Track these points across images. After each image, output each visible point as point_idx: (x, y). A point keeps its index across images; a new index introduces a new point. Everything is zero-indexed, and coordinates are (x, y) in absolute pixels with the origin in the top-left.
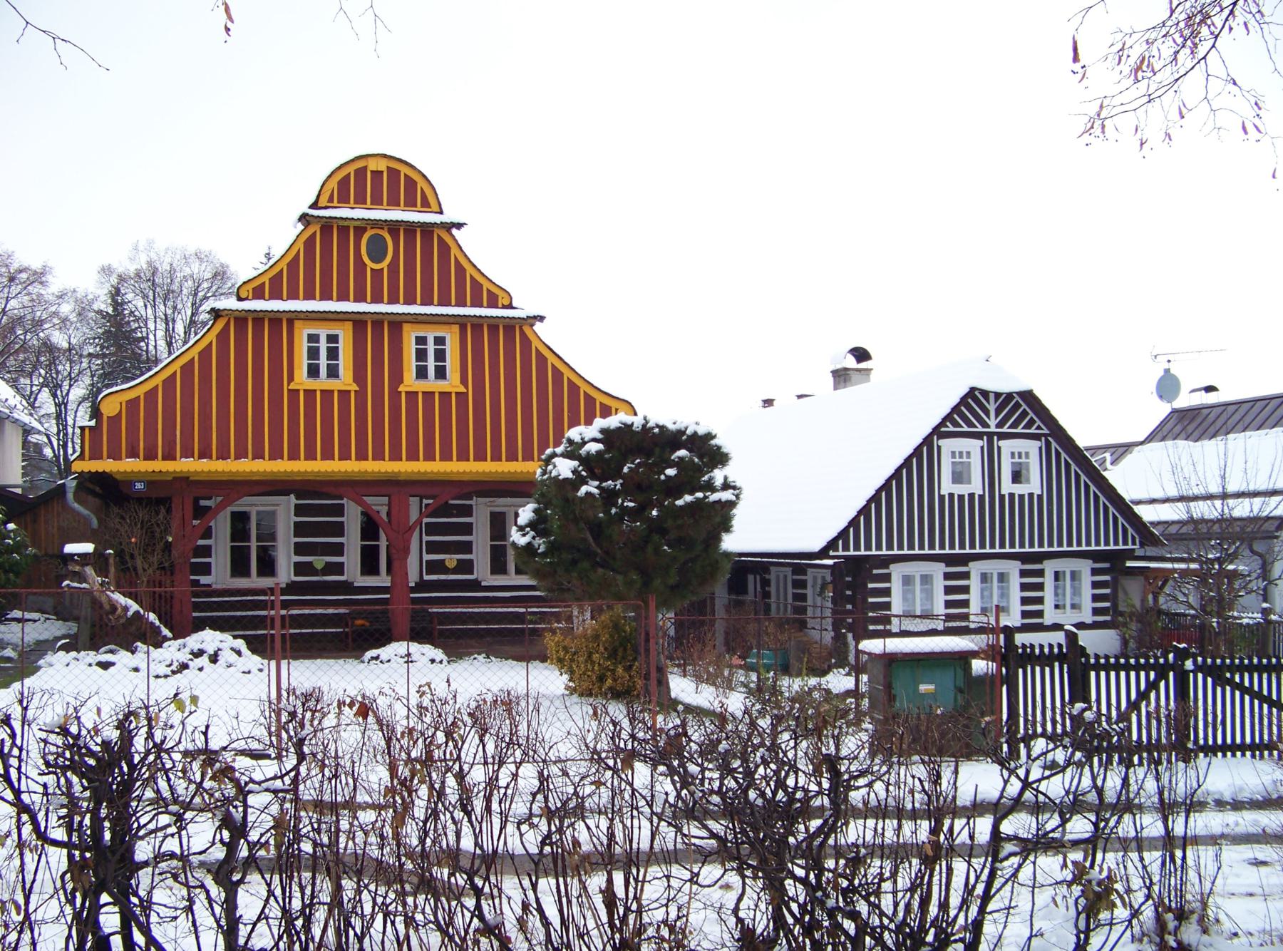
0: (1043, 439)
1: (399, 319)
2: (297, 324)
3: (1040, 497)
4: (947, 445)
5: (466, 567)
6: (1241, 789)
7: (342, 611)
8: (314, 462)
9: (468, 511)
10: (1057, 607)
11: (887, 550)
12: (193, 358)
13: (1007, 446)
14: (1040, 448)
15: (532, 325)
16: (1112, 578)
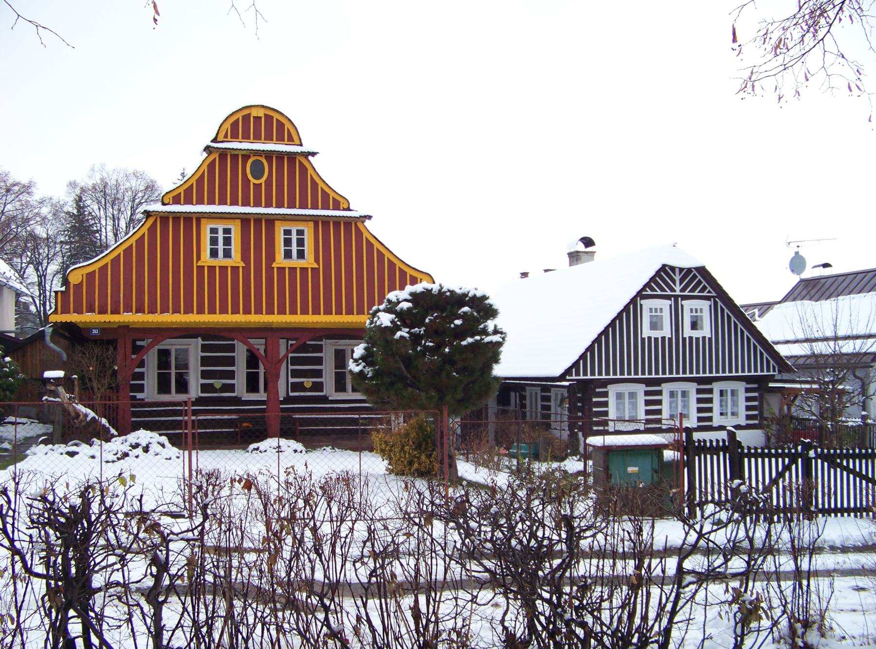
0: (712, 299)
1: (272, 217)
2: (203, 221)
3: (710, 339)
4: (647, 304)
5: (318, 387)
6: (847, 539)
7: (233, 417)
8: (214, 315)
9: (319, 349)
10: (722, 414)
11: (606, 375)
12: (132, 244)
13: (687, 304)
14: (710, 306)
15: (363, 222)
16: (759, 394)
